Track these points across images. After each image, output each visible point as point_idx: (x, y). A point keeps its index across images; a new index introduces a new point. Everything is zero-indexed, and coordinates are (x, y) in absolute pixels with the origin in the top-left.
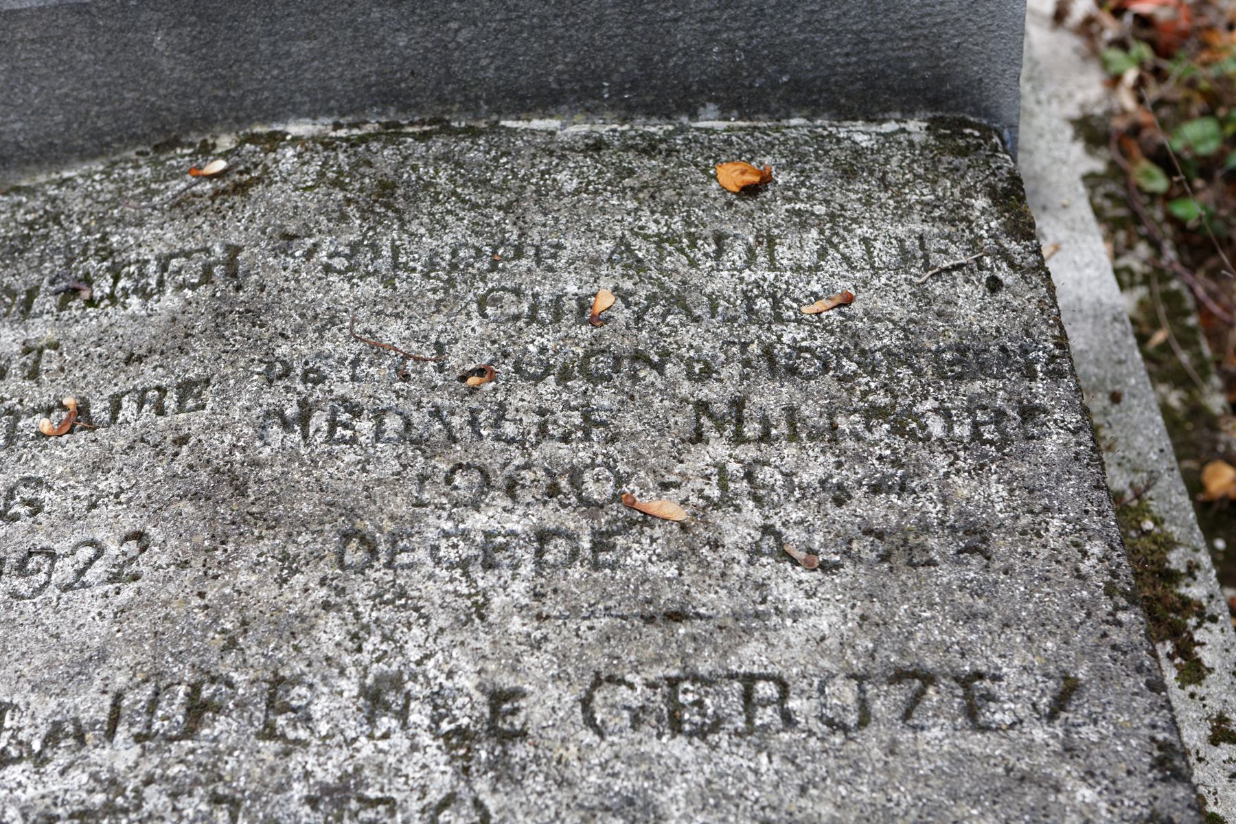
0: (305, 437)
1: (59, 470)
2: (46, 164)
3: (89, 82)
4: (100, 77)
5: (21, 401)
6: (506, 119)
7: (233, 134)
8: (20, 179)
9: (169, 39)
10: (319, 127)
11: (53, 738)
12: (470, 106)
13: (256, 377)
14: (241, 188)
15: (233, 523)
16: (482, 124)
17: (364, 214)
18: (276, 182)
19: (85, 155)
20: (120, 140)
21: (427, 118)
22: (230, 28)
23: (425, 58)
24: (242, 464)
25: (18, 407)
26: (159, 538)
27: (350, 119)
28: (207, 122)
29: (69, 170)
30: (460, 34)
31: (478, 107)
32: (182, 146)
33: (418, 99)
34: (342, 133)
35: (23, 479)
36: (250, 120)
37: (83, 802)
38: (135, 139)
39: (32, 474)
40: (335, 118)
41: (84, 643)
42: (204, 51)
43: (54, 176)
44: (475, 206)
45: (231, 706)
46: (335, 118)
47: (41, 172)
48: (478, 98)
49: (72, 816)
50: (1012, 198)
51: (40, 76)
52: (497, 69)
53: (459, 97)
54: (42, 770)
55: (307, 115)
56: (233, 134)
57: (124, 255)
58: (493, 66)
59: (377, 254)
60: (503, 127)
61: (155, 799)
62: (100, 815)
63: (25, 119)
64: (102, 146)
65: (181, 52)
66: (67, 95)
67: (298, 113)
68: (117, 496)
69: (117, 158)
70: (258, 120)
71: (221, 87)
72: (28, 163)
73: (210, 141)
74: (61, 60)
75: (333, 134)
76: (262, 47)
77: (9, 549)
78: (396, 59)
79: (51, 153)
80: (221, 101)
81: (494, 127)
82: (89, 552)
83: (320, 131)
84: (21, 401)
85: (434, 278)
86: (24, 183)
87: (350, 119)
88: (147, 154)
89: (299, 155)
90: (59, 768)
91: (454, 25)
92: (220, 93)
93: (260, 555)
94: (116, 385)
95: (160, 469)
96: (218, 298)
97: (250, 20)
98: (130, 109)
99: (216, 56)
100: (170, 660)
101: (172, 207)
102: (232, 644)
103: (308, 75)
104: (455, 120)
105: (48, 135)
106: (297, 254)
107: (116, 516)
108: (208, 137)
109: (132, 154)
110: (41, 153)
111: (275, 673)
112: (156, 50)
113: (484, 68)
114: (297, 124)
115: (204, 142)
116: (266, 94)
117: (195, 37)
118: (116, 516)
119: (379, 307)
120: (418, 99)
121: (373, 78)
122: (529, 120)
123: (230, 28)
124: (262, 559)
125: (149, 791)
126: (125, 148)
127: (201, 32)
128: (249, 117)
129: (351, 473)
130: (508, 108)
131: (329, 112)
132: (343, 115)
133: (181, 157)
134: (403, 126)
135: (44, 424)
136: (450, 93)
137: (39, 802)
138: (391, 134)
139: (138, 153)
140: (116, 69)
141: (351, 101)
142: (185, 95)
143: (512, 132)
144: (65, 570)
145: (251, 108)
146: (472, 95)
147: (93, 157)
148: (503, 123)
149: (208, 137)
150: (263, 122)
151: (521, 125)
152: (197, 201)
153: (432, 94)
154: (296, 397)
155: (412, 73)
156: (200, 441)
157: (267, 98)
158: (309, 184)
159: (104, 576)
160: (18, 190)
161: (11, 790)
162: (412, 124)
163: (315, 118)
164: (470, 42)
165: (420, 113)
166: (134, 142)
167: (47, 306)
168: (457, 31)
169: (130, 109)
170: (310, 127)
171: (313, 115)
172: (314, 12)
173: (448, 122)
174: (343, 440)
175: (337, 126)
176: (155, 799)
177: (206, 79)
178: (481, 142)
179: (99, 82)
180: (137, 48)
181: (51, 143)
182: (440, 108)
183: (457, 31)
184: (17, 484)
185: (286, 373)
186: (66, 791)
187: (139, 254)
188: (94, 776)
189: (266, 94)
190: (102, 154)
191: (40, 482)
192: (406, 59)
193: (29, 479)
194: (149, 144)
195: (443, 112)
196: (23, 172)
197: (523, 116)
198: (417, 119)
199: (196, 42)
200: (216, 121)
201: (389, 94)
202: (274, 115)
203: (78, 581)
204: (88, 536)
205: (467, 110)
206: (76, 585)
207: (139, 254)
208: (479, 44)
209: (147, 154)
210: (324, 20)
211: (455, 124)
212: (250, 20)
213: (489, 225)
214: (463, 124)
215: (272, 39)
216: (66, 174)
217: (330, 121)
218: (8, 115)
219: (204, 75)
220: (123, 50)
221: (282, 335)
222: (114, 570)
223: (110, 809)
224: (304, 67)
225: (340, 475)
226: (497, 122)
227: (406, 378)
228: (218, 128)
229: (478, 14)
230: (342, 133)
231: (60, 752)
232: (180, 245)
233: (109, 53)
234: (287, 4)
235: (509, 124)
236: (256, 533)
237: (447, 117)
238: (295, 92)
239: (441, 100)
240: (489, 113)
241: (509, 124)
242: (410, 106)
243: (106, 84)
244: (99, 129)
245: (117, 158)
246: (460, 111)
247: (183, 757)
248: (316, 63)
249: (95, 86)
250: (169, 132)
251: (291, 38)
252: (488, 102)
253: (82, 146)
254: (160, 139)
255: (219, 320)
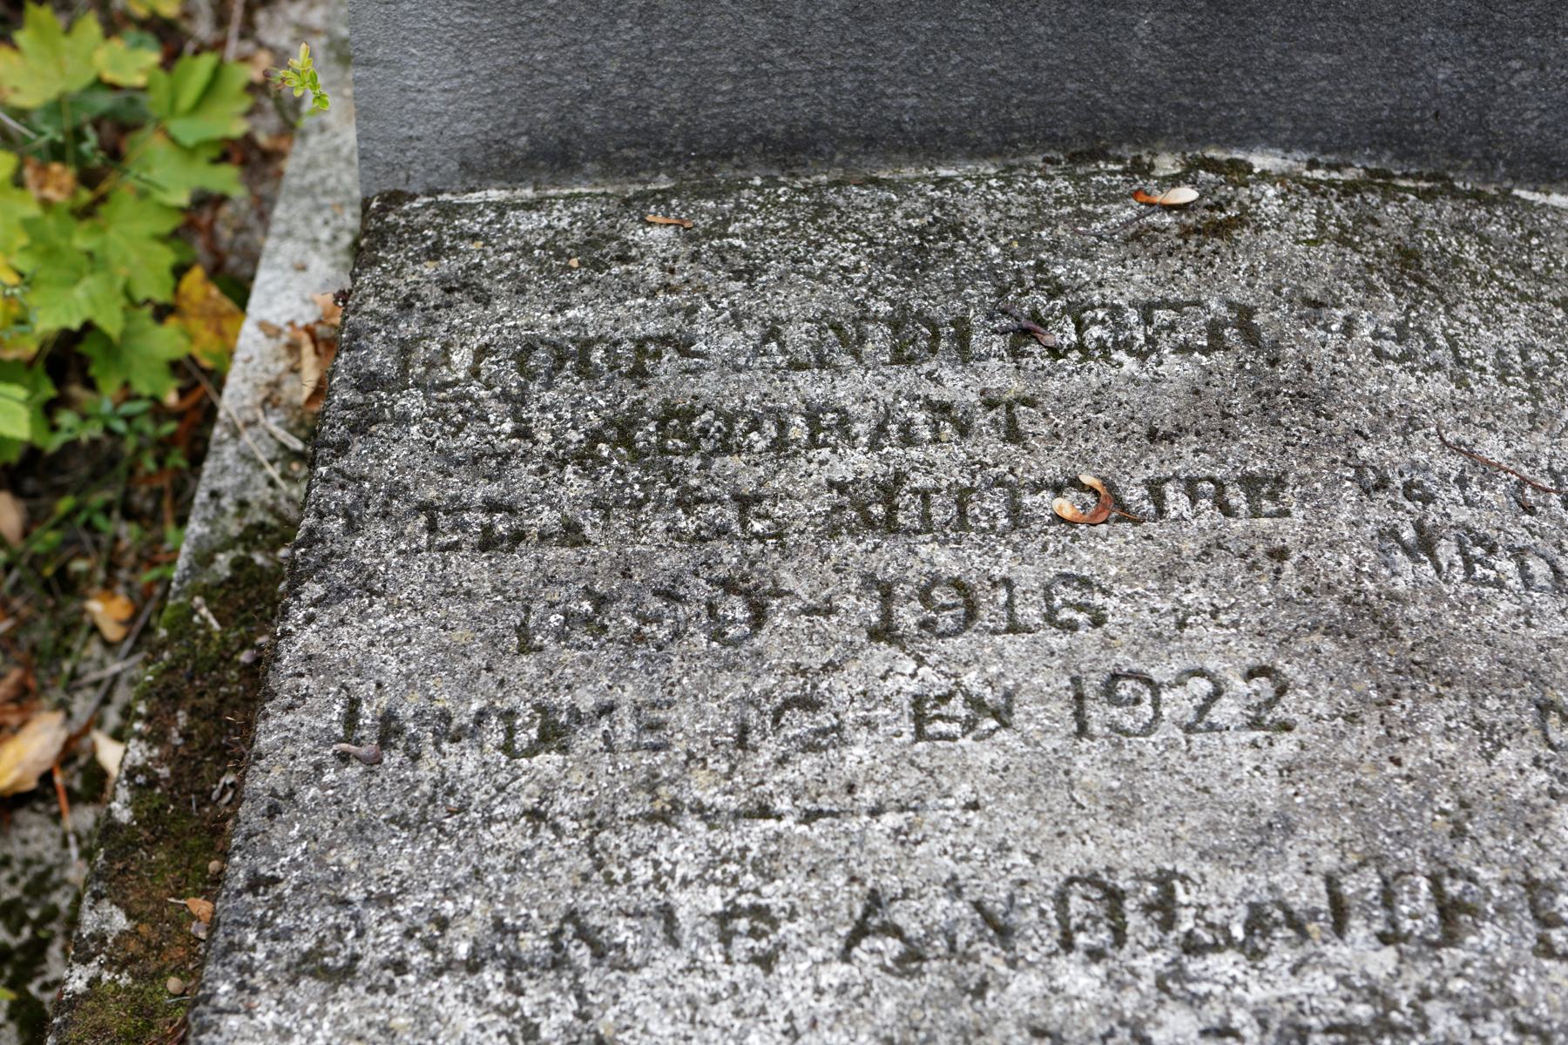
0: (1438, 569)
1: (1113, 571)
2: (921, 156)
3: (1029, 63)
4: (1046, 58)
5: (1012, 471)
6: (1521, 188)
7: (1179, 154)
8: (878, 168)
9: (1159, 24)
10: (1290, 162)
11: (1257, 921)
12: (1485, 166)
13: (1348, 484)
14: (1220, 229)
15: (1398, 672)
16: (1491, 190)
17: (1396, 285)
18: (1267, 228)
19: (977, 151)
20: (1032, 139)
21: (1426, 172)
22: (1241, 23)
23: (1461, 97)
24: (1379, 595)
25: (1010, 477)
26: (1303, 679)
27: (1332, 158)
28: (1152, 135)
29: (948, 168)
30: (1517, 77)
31: (1494, 167)
32: (1107, 159)
33: (1426, 147)
34: (1318, 174)
35: (1060, 575)
36: (1206, 141)
37: (1341, 1013)
38: (1052, 141)
39: (1073, 570)
40: (1312, 155)
41: (1253, 805)
42: (1194, 46)
43: (925, 171)
44: (1524, 297)
45: (1492, 911)
46: (1312, 155)
47: (910, 164)
48: (1500, 156)
49: (1330, 1029)
50: (459, 206)
51: (970, 44)
52: (1541, 126)
53: (1477, 153)
54: (1261, 965)
55: (1281, 145)
56: (1179, 154)
57: (1083, 295)
58: (1537, 122)
59: (1431, 345)
60: (1518, 197)
61: (1443, 1020)
62: (1373, 1032)
63: (924, 94)
64: (1006, 143)
65: (1165, 42)
66: (994, 73)
67: (1270, 140)
68: (1214, 615)
69: (1016, 162)
70: (1217, 141)
71: (1193, 94)
72: (898, 150)
73: (1146, 159)
74: (1009, 28)
75: (1307, 174)
76: (1269, 53)
77: (1083, 666)
78: (1425, 94)
79: (933, 142)
80: (1178, 108)
81: (1506, 197)
82: (1205, 686)
83: (1290, 167)
84: (1012, 471)
85: (1513, 384)
86: (883, 175)
87: (1332, 158)
88: (1059, 162)
89: (1283, 196)
90: (1287, 966)
91: (1516, 64)
92: (1186, 101)
93: (1449, 718)
94: (1147, 467)
95: (1263, 588)
96: (1250, 372)
97: (1272, 17)
98: (1063, 103)
99: (1206, 55)
100: (1388, 840)
101: (1127, 241)
102: (1458, 833)
103: (1307, 97)
104: (1460, 179)
105: (943, 119)
106: (1334, 327)
107: (1225, 643)
108: (1143, 153)
109: (1038, 160)
110: (922, 140)
111: (1528, 876)
112: (1135, 35)
113: (1525, 123)
114: (1263, 155)
115: (1137, 161)
116: (1243, 111)
117: (1191, 28)
118: (1225, 643)
119: (1462, 413)
120: (1426, 147)
121: (1385, 113)
122: (1548, 194)
123: (1241, 23)
124: (1452, 724)
125: (1432, 1008)
126: (1032, 152)
127: (1202, 23)
128: (1207, 135)
129: (1515, 627)
130: (1529, 175)
131: (1308, 146)
132: (1324, 152)
133: (1107, 173)
134: (1394, 176)
135: (1066, 505)
136: (1469, 146)
137: (1278, 1006)
138: (1382, 182)
139: (1047, 160)
140: (1072, 51)
141: (1345, 136)
142: (1141, 98)
143: (1528, 205)
144: (1180, 703)
145: (1206, 122)
146: (1494, 152)
147: (986, 155)
148: (1516, 192)
149: (1143, 153)
150: (1221, 145)
151: (1538, 198)
152: (1162, 237)
153: (1446, 144)
154: (1408, 518)
155: (1437, 114)
156: (1306, 558)
157: (1242, 116)
158: (1311, 236)
159: (1242, 720)
160: (878, 183)
161: (1227, 987)
162: (1405, 176)
163: (1288, 151)
164: (1525, 88)
165: (1420, 163)
166: (1047, 144)
167: (995, 348)
168: (1516, 71)
169: (1063, 103)
170: (1278, 161)
171: (1287, 147)
172: (1356, 22)
173: (1452, 180)
174: (1485, 582)
175: (1313, 165)
176: (1443, 1020)
177: (1178, 82)
178: (1499, 213)
179: (1043, 63)
180: (1112, 29)
181: (942, 130)
182: (1448, 162)
183: (1516, 71)
184: (1053, 581)
185: (1383, 484)
186: (1310, 996)
187: (1103, 296)
188: (1343, 980)
189: (1243, 111)
190: (1000, 153)
191: (1085, 583)
192: (1438, 96)
193: (1066, 576)
194: (1065, 150)
195: (1448, 168)
196: (887, 160)
197: (1542, 187)
198: (1413, 170)
199: (1189, 34)
200: (1163, 135)
201: (1398, 138)
202: (1240, 139)
203: (1199, 721)
204: (1192, 663)
205: (1480, 169)
206: (1201, 726)
207: (1103, 296)
208: (1535, 92)
209: (1059, 162)
210: (1361, 33)
211: (1459, 185)
212: (1272, 17)
213: (1551, 325)
214: (1469, 186)
215: (1286, 45)
216: (943, 172)
217: (1306, 157)
218: (905, 85)
219: (1178, 75)
220: (1093, 29)
221: (1360, 433)
222: (1252, 714)
223: (1384, 1026)
224: (1308, 86)
225: (1503, 627)
226: (1510, 190)
227: (1530, 510)
228: (1161, 144)
229: (1552, 56)
230: (1318, 174)
231: (1277, 943)
232: (1160, 292)
233: (1075, 29)
234: (1326, 6)
235: (1524, 194)
236: (1432, 688)
237: (1451, 175)
238: (1280, 114)
239: (1454, 153)
240: (1505, 177)
241: (1524, 194)
242: (1412, 154)
243: (1050, 68)
244: (1012, 121)
245: (1016, 162)
246: (1470, 169)
247: (1460, 969)
248: (1324, 83)
249: (1036, 67)
250: (1098, 138)
251: (1310, 47)
252: (1508, 164)
253: (979, 139)
254: (1081, 146)
255: (1264, 401)
